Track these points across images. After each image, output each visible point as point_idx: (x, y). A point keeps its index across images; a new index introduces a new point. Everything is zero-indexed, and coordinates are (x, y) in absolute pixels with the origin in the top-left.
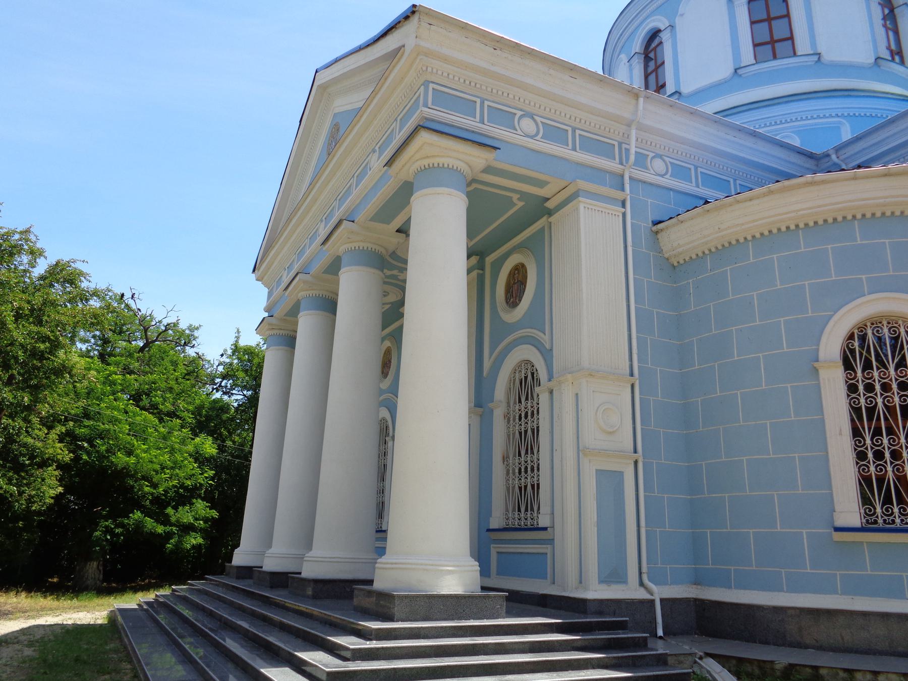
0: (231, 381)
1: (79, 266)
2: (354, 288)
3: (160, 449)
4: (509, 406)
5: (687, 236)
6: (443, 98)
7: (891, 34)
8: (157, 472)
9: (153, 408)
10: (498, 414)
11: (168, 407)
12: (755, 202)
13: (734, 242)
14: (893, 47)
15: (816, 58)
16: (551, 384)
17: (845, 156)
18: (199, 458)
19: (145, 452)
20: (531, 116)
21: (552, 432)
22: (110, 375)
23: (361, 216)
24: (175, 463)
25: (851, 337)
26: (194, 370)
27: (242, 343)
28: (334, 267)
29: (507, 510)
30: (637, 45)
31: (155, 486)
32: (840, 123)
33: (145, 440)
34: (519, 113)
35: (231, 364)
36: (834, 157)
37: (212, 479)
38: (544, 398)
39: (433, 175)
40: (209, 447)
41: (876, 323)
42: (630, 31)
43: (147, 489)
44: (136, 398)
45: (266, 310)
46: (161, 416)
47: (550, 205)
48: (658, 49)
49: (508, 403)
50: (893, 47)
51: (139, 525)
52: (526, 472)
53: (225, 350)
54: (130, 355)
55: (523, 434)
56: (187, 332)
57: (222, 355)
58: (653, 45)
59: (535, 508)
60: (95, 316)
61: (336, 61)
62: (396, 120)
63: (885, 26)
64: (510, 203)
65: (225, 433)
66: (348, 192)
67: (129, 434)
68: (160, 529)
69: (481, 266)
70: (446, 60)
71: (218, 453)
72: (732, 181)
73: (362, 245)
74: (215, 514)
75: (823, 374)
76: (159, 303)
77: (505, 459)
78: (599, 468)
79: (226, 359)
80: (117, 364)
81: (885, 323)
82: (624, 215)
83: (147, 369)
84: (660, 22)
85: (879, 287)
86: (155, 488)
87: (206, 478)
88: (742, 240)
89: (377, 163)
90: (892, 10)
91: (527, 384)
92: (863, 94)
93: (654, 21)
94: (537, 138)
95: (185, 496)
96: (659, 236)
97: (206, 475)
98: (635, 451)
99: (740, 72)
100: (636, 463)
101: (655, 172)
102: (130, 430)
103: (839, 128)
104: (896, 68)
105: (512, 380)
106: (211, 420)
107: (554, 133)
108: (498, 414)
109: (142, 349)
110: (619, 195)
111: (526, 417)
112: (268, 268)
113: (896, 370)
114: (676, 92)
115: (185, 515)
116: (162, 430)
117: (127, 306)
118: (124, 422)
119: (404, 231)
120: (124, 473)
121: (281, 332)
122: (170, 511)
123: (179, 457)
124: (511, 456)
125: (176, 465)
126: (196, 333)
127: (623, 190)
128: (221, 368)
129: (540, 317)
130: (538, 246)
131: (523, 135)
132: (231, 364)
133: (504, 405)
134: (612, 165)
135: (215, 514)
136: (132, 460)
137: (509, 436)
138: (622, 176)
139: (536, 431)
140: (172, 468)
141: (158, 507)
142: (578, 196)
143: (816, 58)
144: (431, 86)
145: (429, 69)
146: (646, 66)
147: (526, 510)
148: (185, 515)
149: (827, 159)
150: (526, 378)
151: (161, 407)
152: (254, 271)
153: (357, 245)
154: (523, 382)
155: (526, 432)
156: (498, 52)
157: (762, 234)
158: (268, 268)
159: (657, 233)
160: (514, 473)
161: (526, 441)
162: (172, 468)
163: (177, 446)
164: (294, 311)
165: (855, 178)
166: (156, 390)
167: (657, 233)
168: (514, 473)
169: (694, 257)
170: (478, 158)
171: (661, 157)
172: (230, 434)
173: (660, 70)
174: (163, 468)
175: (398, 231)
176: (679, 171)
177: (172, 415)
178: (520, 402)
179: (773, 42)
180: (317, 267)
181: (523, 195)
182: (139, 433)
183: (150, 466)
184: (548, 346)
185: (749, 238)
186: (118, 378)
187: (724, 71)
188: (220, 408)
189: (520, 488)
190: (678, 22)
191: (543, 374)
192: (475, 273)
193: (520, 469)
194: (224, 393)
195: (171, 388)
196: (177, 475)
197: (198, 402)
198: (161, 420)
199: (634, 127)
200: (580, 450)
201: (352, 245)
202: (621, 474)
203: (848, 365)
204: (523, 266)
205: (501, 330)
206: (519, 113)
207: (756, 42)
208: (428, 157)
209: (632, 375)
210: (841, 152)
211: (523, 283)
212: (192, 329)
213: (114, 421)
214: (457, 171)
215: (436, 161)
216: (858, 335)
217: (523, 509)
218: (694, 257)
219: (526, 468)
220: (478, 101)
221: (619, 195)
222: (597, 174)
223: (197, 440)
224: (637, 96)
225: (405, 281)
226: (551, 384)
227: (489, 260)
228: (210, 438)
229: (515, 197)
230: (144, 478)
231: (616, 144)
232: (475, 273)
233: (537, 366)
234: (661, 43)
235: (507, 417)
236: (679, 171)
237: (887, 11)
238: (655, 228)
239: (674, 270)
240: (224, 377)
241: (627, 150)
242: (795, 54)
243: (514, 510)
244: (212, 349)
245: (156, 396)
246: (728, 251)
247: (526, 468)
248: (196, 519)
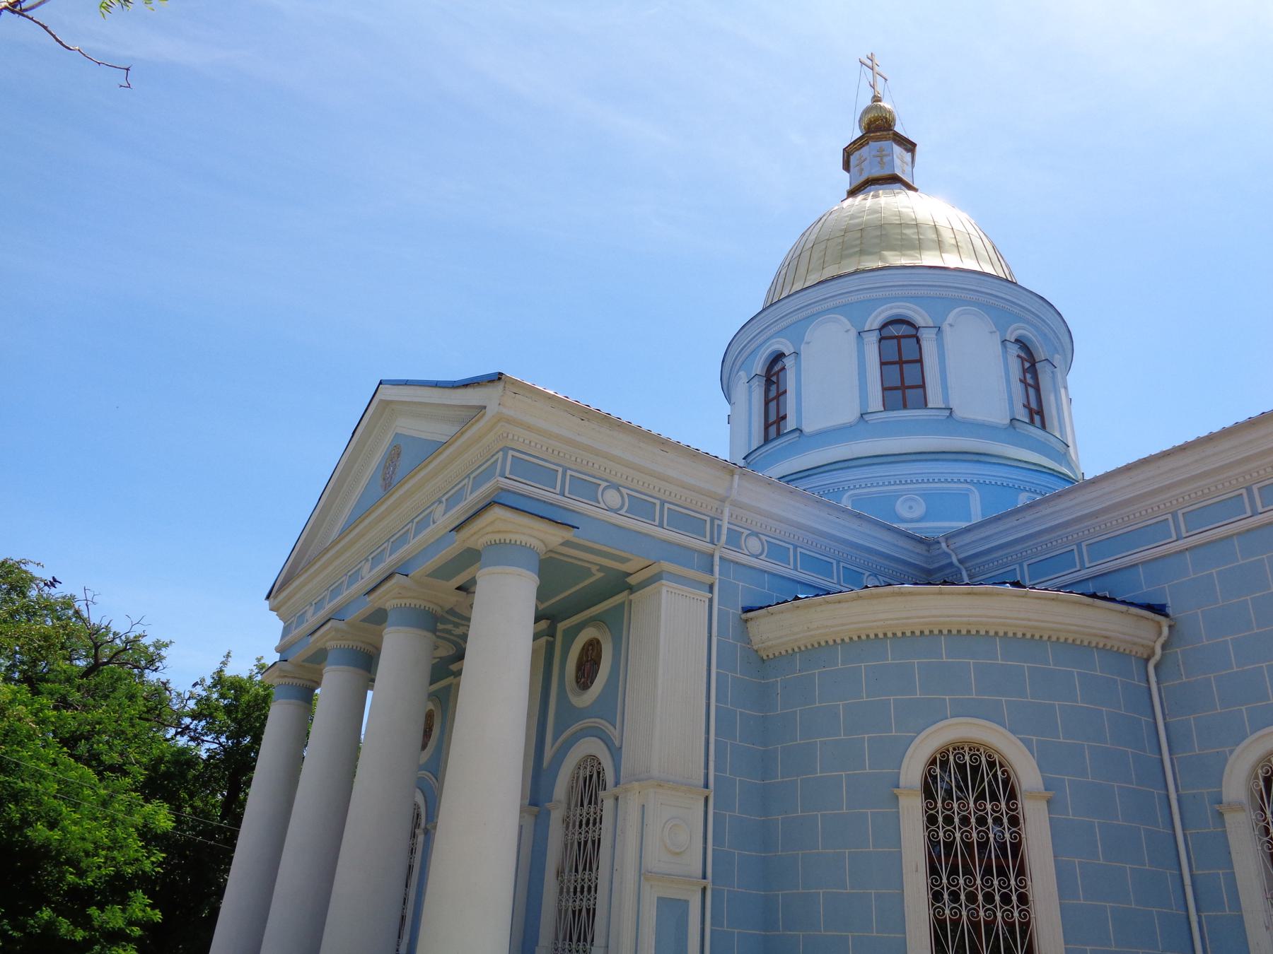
0: (203, 723)
1: (30, 568)
2: (400, 651)
3: (96, 819)
4: (569, 808)
5: (780, 629)
6: (526, 467)
7: (1032, 391)
8: (87, 854)
9: (92, 759)
10: (557, 816)
11: (116, 758)
12: (842, 605)
13: (823, 643)
14: (1034, 405)
15: (947, 413)
16: (616, 790)
17: (957, 545)
18: (148, 836)
19: (75, 823)
20: (617, 487)
21: (614, 847)
22: (41, 710)
23: (417, 571)
24: (115, 840)
25: (933, 762)
26: (156, 706)
27: (229, 672)
28: (379, 617)
29: (557, 939)
30: (759, 366)
31: (81, 873)
32: (968, 490)
33: (76, 806)
34: (604, 484)
35: (208, 699)
36: (944, 545)
37: (160, 865)
38: (608, 805)
39: (504, 552)
40: (163, 819)
41: (958, 748)
42: (753, 347)
43: (70, 878)
44: (69, 742)
45: (278, 650)
46: (102, 769)
47: (632, 580)
48: (781, 374)
49: (569, 804)
50: (1034, 405)
51: (50, 926)
52: (582, 892)
53: (203, 680)
54: (69, 680)
55: (582, 845)
56: (151, 649)
57: (195, 685)
58: (776, 369)
59: (589, 940)
60: (46, 638)
61: (406, 383)
62: (468, 476)
63: (1023, 381)
64: (588, 573)
65: (183, 795)
66: (403, 539)
67: (55, 797)
68: (79, 935)
69: (551, 632)
70: (529, 428)
71: (174, 828)
72: (835, 563)
73: (413, 602)
74: (157, 916)
75: (903, 802)
76: (115, 608)
77: (560, 873)
78: (661, 895)
79: (199, 690)
80: (51, 694)
81: (967, 749)
82: (711, 600)
83: (91, 701)
84: (787, 348)
85: (965, 710)
86: (81, 878)
87: (153, 863)
88: (831, 643)
89: (444, 519)
90: (1033, 365)
91: (591, 785)
92: (994, 460)
93: (778, 342)
94: (622, 512)
95: (118, 889)
96: (749, 624)
97: (153, 859)
98: (704, 877)
99: (867, 417)
100: (704, 890)
101: (751, 552)
102: (59, 791)
103: (967, 495)
104: (1035, 432)
105: (575, 778)
106: (169, 778)
107: (641, 507)
108: (557, 816)
109: (87, 673)
110: (707, 578)
111: (588, 824)
112: (289, 598)
113: (975, 802)
114: (797, 429)
115: (114, 917)
116: (103, 792)
117: (77, 612)
118: (51, 778)
119: (466, 589)
120: (43, 853)
121: (295, 681)
122: (93, 911)
123: (119, 831)
124: (567, 870)
125: (116, 844)
126: (163, 652)
127: (712, 572)
128: (192, 704)
129: (610, 707)
130: (616, 622)
131: (606, 509)
132: (208, 699)
133: (564, 805)
134: (703, 545)
135: (157, 916)
136: (56, 835)
137: (566, 845)
138: (712, 556)
139: (597, 844)
140: (109, 849)
141: (77, 902)
142: (661, 578)
143: (947, 413)
144: (511, 453)
145: (510, 436)
146: (767, 391)
147: (579, 940)
148: (114, 917)
149: (937, 546)
150: (591, 776)
151: (104, 757)
152: (268, 597)
153: (408, 602)
154: (588, 780)
155: (586, 842)
156: (586, 423)
157: (851, 639)
158: (289, 598)
159: (746, 621)
160: (568, 892)
161: (585, 853)
162: (109, 849)
163: (120, 816)
164: (319, 657)
165: (940, 593)
166: (99, 733)
167: (746, 621)
168: (568, 892)
169: (784, 653)
170: (554, 536)
171: (756, 534)
172: (192, 796)
173: (781, 398)
174: (97, 848)
175: (458, 588)
176: (777, 552)
177: (120, 770)
178: (582, 805)
179: (903, 387)
180: (354, 614)
181: (602, 568)
182: (69, 793)
183: (80, 845)
184: (617, 743)
185: (839, 641)
186: (51, 714)
187: (848, 415)
188: (184, 760)
189: (574, 912)
190: (803, 349)
191: (609, 776)
192: (543, 640)
193: (575, 888)
194: (192, 739)
195: (123, 732)
196: (114, 859)
197: (156, 752)
198: (99, 773)
199: (727, 504)
200: (643, 874)
201: (403, 602)
202: (685, 904)
203: (928, 793)
204: (598, 642)
205: (568, 714)
206: (604, 484)
207: (886, 385)
208: (499, 532)
209: (706, 786)
210: (951, 542)
211: (596, 663)
212: (159, 645)
213: (39, 777)
214: (531, 549)
215: (508, 537)
216: (939, 761)
217: (575, 938)
218: (784, 653)
219: (582, 887)
220: (560, 470)
221: (707, 578)
222: (682, 554)
223: (149, 808)
224: (732, 473)
225: (464, 637)
226: (616, 790)
227: (561, 626)
228: (166, 806)
229: (594, 569)
230: (69, 862)
231: (708, 519)
232: (543, 640)
233: (602, 761)
234: (783, 369)
235: (566, 822)
236: (777, 552)
237: (1027, 365)
238: (744, 616)
239: (763, 664)
240: (195, 716)
241: (720, 526)
242: (925, 405)
243: (564, 939)
244: (184, 672)
245: (99, 742)
246: (817, 652)
247: (582, 887)
248: (131, 923)
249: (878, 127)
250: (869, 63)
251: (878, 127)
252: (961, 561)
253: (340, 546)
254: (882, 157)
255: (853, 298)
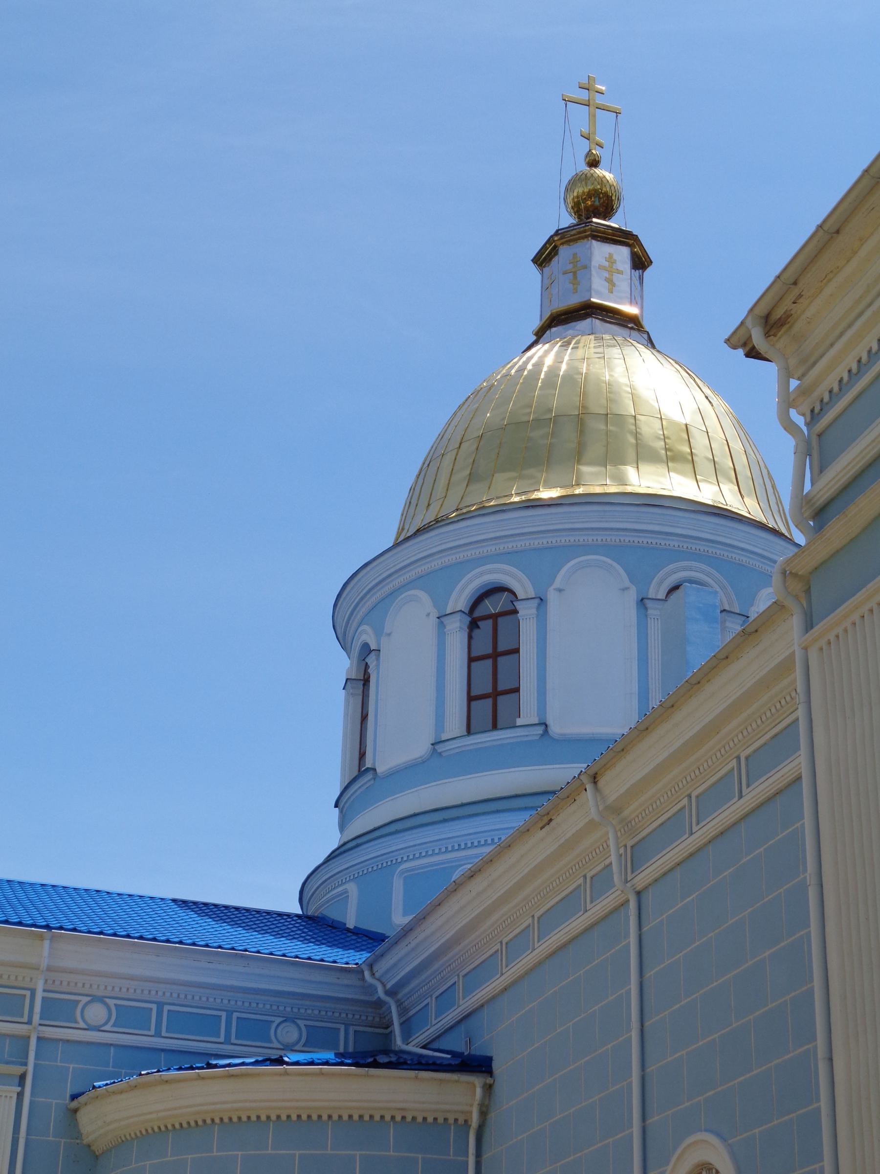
5: (119, 1112)
15: (543, 727)
82: (20, 1095)
143: (540, 730)
167: (75, 1111)
176: (129, 1016)
187: (420, 748)
238: (74, 1104)
249: (594, 206)
250: (584, 95)
251: (594, 206)
252: (391, 993)
253: (828, 487)
254: (579, 271)
255: (436, 563)
